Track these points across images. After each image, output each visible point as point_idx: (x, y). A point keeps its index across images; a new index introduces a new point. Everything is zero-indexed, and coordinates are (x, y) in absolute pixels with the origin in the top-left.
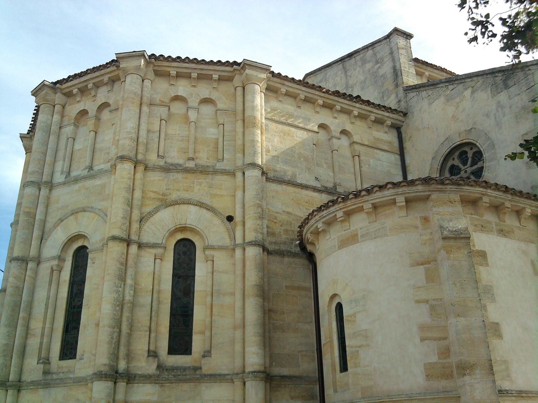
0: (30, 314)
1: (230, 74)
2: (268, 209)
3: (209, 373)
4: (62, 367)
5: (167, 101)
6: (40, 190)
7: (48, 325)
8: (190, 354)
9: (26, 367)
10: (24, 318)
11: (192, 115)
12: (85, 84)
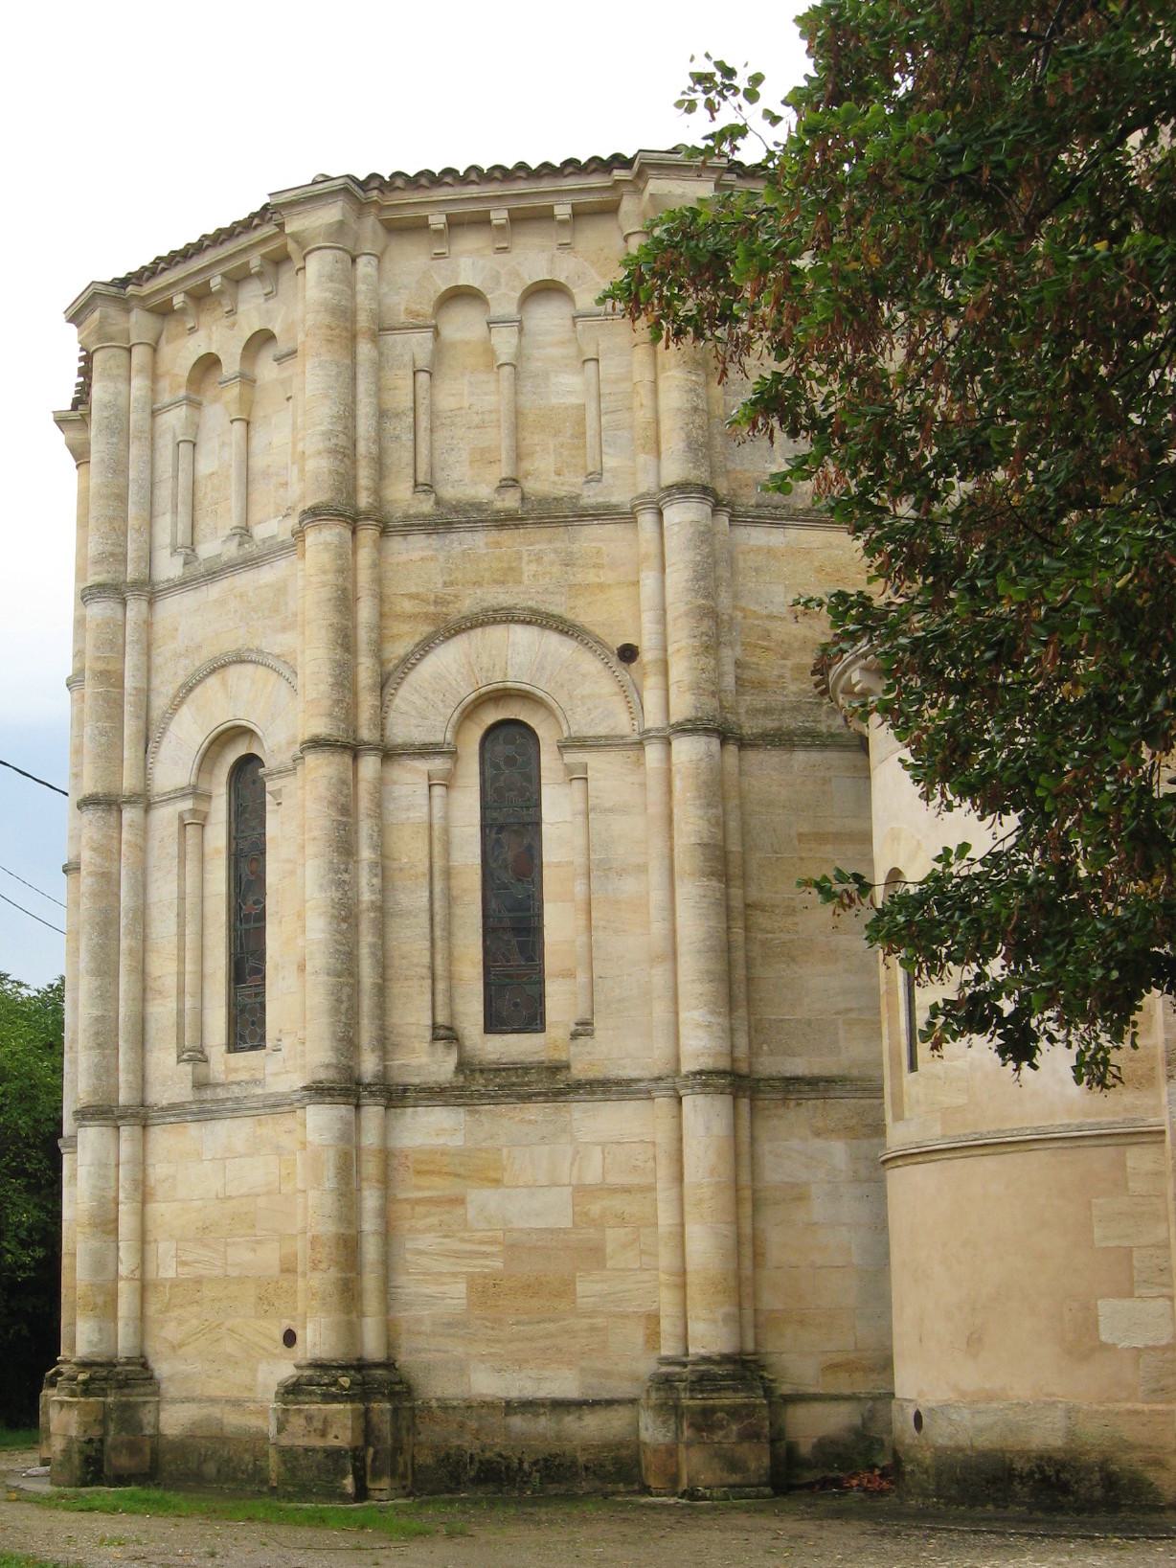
0: (145, 939)
1: (606, 196)
2: (743, 610)
3: (591, 1075)
4: (236, 1070)
5: (428, 309)
6: (125, 605)
7: (190, 967)
8: (543, 1030)
9: (154, 1073)
10: (131, 951)
11: (504, 342)
12: (199, 280)
